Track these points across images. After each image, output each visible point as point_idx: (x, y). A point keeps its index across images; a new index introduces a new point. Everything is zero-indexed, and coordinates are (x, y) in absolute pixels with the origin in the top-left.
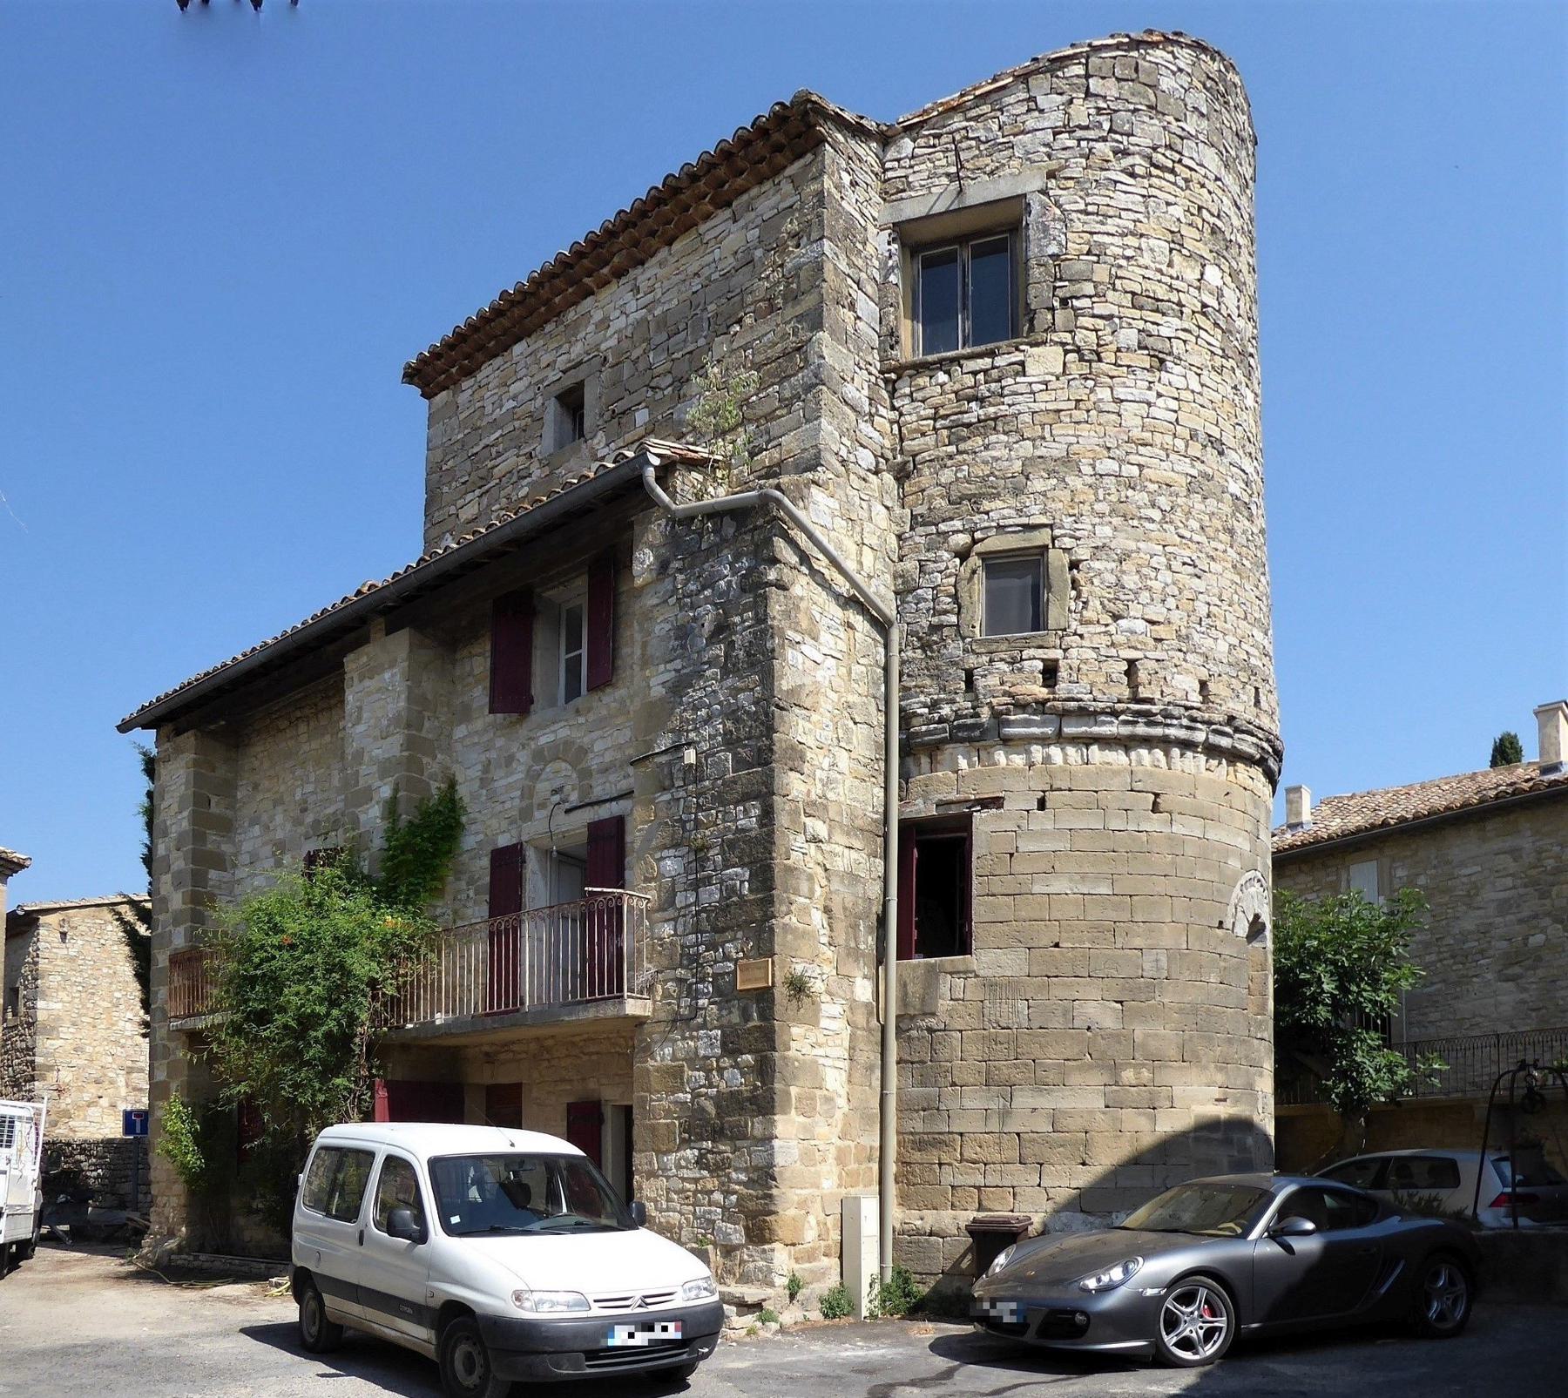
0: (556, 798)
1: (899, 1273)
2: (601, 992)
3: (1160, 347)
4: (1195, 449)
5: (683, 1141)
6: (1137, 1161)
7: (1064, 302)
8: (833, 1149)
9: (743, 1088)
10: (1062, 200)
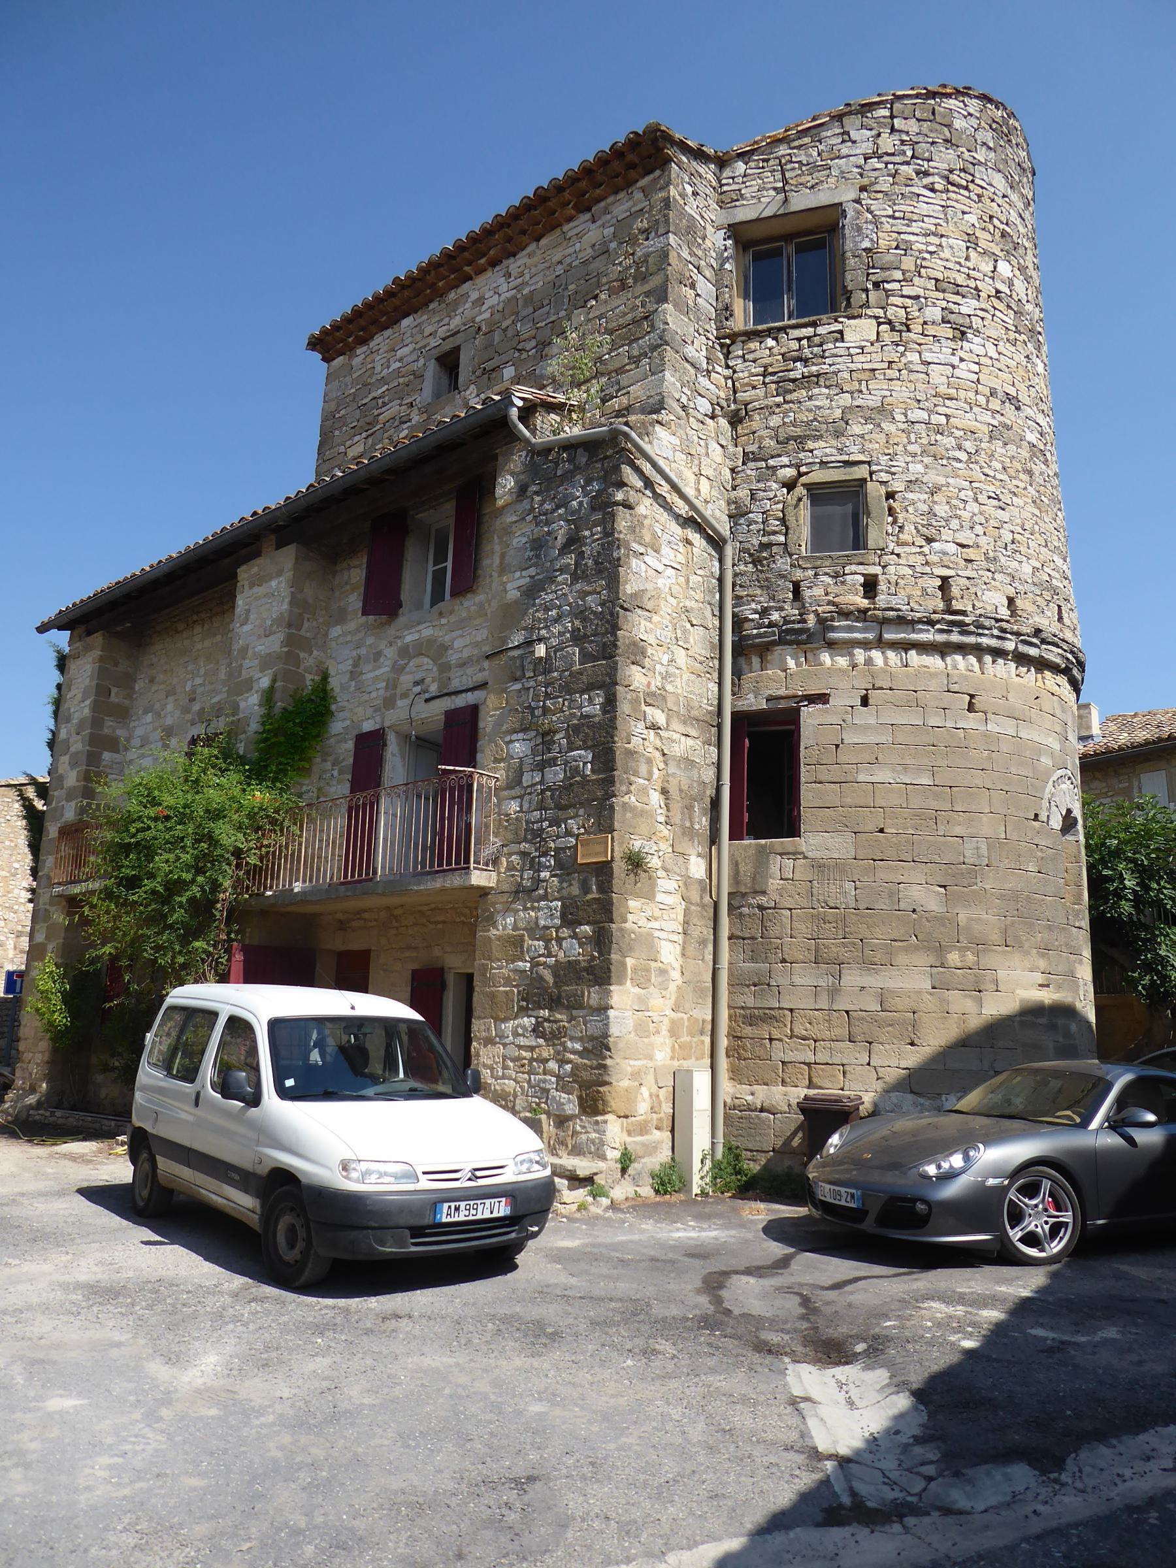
0: (418, 689)
1: (729, 1149)
2: (449, 863)
3: (961, 322)
4: (995, 404)
5: (521, 1008)
6: (965, 1043)
7: (876, 285)
8: (666, 1021)
9: (581, 958)
10: (873, 208)
